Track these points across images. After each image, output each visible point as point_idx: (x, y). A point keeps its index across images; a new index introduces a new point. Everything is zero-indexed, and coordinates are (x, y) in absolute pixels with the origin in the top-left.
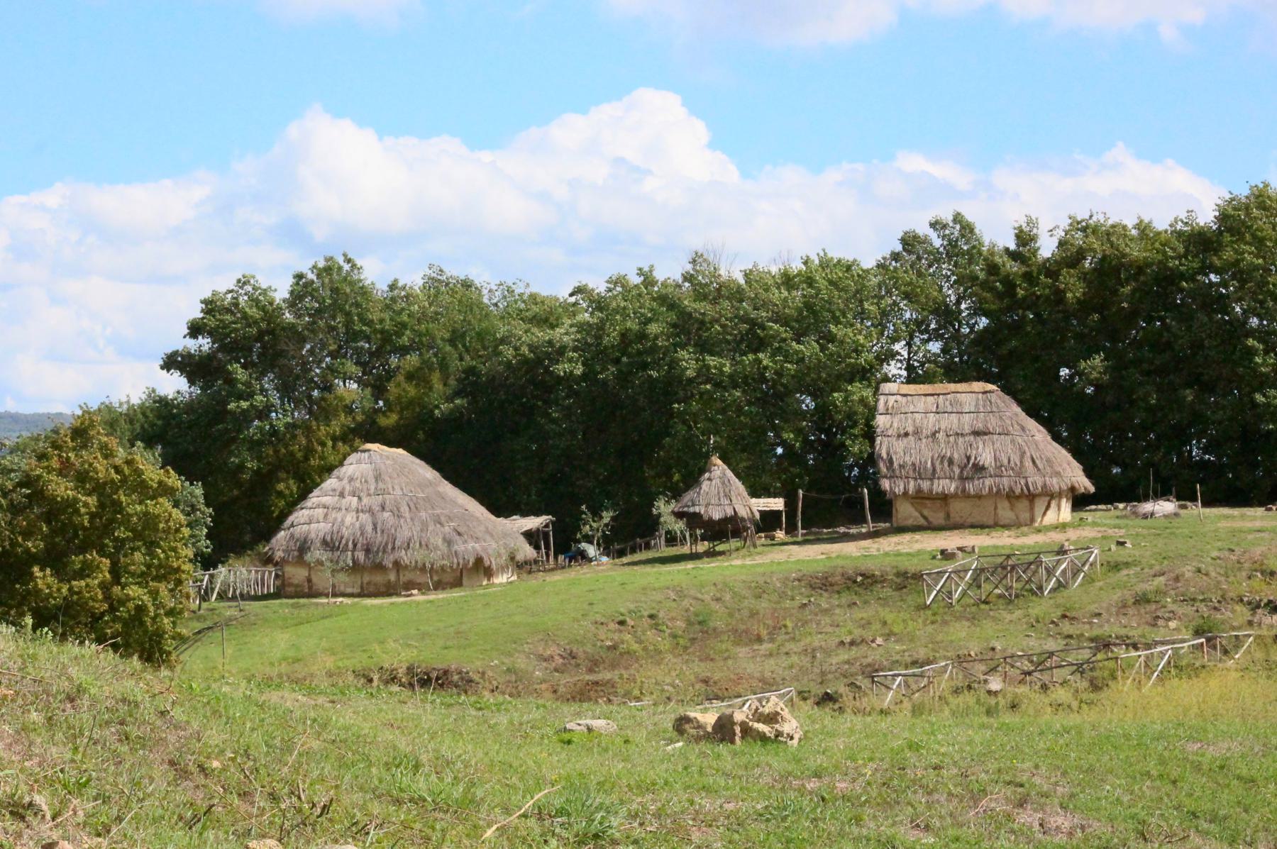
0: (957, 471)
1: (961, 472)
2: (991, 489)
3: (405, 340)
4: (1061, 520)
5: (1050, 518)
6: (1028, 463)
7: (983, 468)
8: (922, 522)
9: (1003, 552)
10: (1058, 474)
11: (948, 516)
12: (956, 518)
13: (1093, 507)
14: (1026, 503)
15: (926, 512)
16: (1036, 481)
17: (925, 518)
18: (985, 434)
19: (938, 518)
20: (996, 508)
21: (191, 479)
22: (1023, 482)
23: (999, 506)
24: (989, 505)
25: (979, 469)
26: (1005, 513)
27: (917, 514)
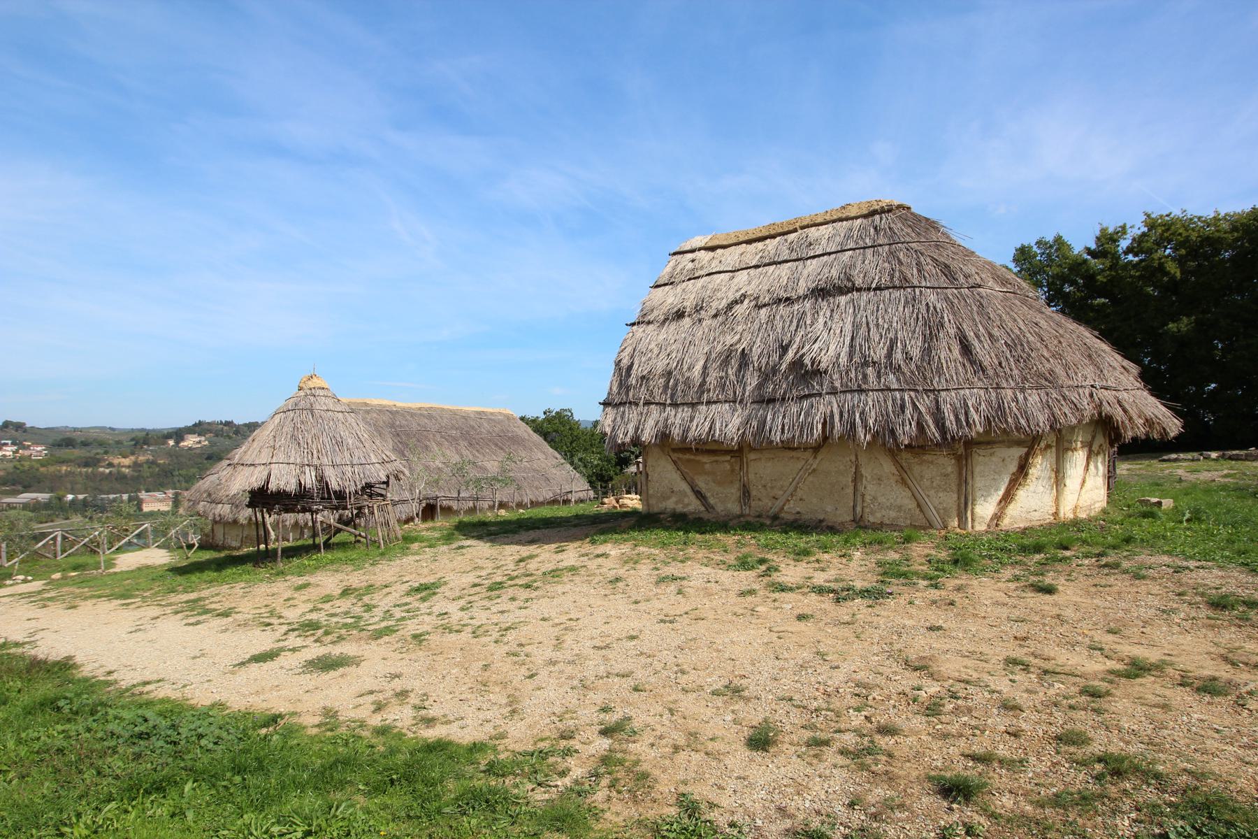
0: (752, 381)
1: (760, 386)
2: (827, 423)
3: (1099, 767)
4: (1067, 512)
5: (1034, 503)
6: (948, 352)
7: (817, 373)
8: (692, 505)
9: (339, 554)
10: (1048, 380)
11: (746, 493)
12: (763, 502)
13: (1174, 456)
14: (947, 464)
15: (702, 484)
16: (967, 400)
17: (699, 495)
18: (842, 291)
19: (726, 501)
20: (857, 478)
21: (1246, 448)
22: (925, 404)
23: (866, 471)
24: (835, 466)
25: (806, 375)
26: (885, 494)
27: (684, 486)
